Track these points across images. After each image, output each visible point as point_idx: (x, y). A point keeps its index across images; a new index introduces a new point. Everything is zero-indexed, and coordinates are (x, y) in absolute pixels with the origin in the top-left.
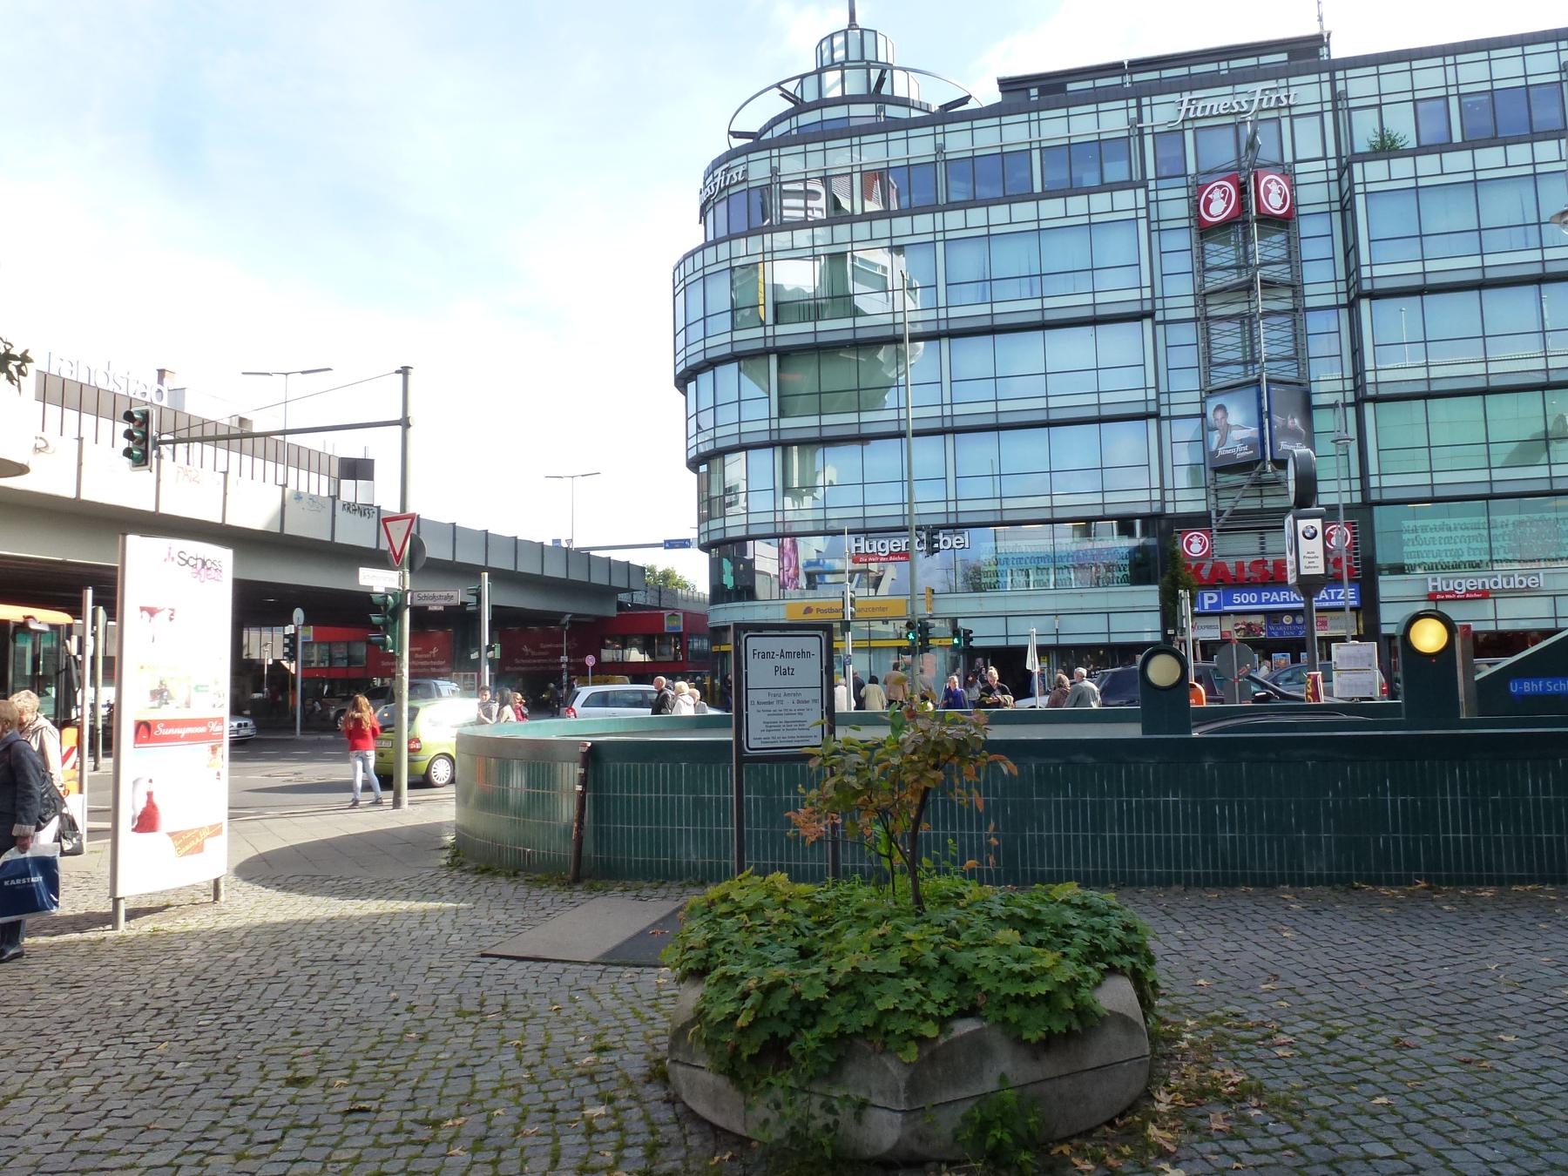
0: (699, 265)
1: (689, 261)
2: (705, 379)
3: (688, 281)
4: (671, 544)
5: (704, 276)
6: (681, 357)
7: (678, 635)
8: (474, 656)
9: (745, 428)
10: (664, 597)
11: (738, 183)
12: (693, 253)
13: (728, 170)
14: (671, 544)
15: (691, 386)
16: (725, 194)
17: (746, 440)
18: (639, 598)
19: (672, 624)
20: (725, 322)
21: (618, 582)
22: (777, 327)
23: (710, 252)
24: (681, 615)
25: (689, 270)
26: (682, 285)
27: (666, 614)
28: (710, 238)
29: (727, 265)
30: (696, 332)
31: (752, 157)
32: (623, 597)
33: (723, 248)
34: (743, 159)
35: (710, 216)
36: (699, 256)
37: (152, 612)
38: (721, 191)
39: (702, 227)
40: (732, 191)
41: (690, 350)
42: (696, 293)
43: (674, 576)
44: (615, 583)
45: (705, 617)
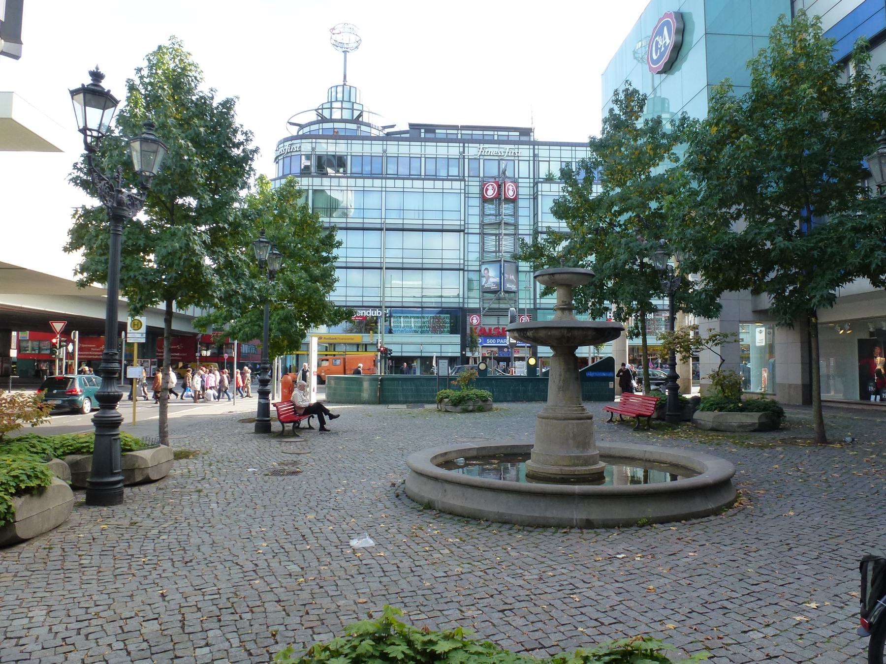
16: (290, 154)
31: (303, 141)
34: (299, 141)
35: (281, 162)
40: (293, 154)
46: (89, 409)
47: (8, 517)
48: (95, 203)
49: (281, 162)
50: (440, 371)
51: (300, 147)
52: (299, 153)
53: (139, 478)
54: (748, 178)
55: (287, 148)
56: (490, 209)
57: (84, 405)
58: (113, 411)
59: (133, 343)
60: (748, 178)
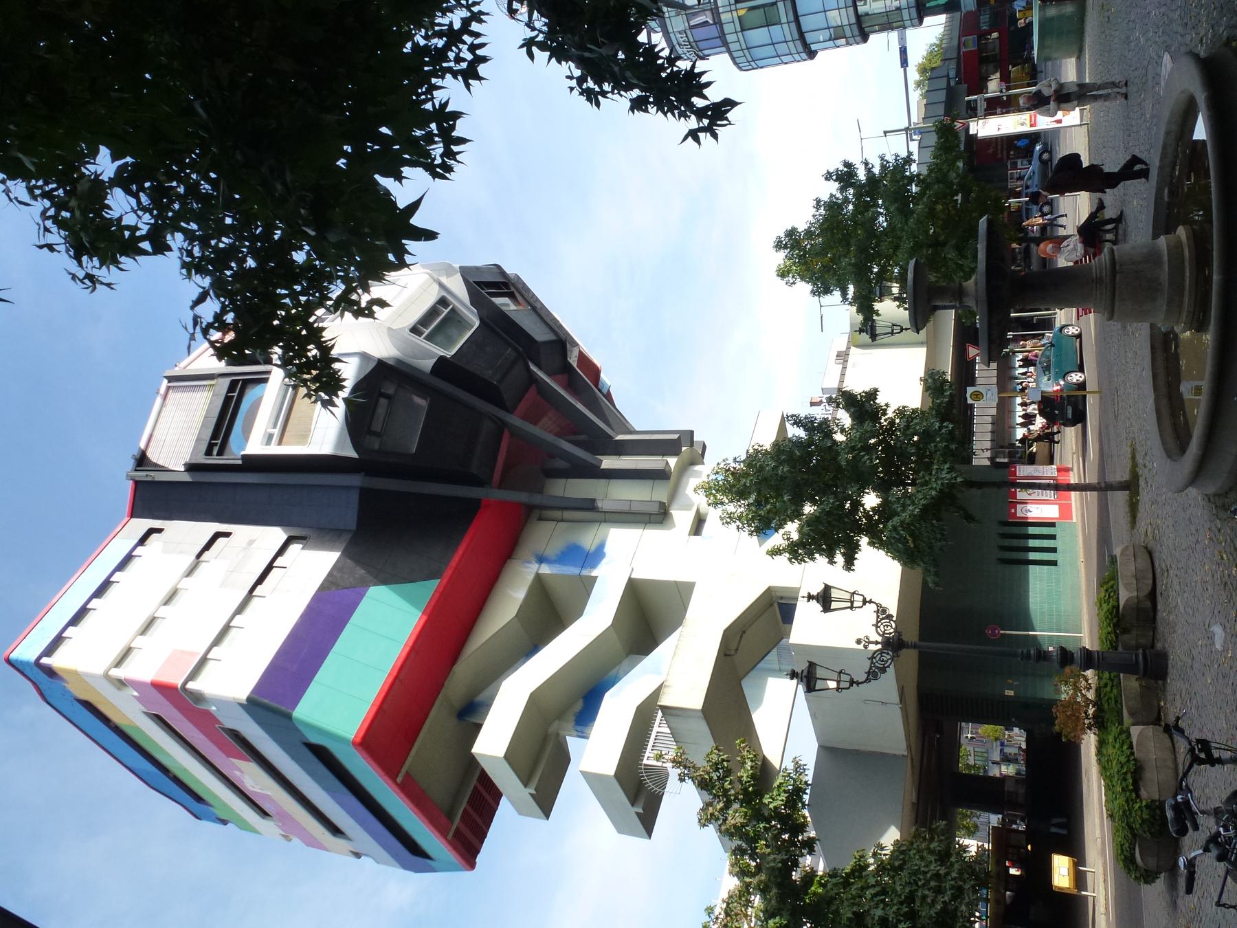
0: (741, 53)
1: (738, 60)
2: (809, 37)
3: (750, 59)
4: (904, 63)
5: (748, 49)
6: (797, 57)
7: (980, 38)
8: (1005, 98)
9: (789, 38)
10: (948, 56)
11: (687, 36)
12: (733, 59)
13: (680, 45)
14: (904, 63)
15: (813, 47)
16: (694, 44)
17: (796, 36)
18: (952, 74)
19: (971, 44)
20: (776, 29)
21: (943, 83)
22: (737, 5)
23: (733, 47)
24: (963, 39)
25: (744, 59)
26: (752, 63)
27: (963, 49)
28: (724, 49)
29: (740, 34)
30: (782, 48)
31: (670, 30)
32: (952, 83)
33: (730, 38)
34: (672, 36)
35: (706, 52)
36: (735, 54)
37: (999, 129)
38: (692, 47)
39: (711, 58)
40: (692, 40)
41: (794, 51)
42: (758, 53)
43: (923, 63)
44: (944, 85)
45: (969, 13)
46: (1080, 374)
47: (1153, 807)
48: (864, 541)
49: (706, 52)
50: (1037, 568)
51: (680, 33)
52: (688, 32)
53: (1148, 604)
54: (779, 495)
55: (685, 50)
56: (856, 604)
57: (1075, 381)
58: (1075, 655)
59: (999, 397)
60: (779, 495)
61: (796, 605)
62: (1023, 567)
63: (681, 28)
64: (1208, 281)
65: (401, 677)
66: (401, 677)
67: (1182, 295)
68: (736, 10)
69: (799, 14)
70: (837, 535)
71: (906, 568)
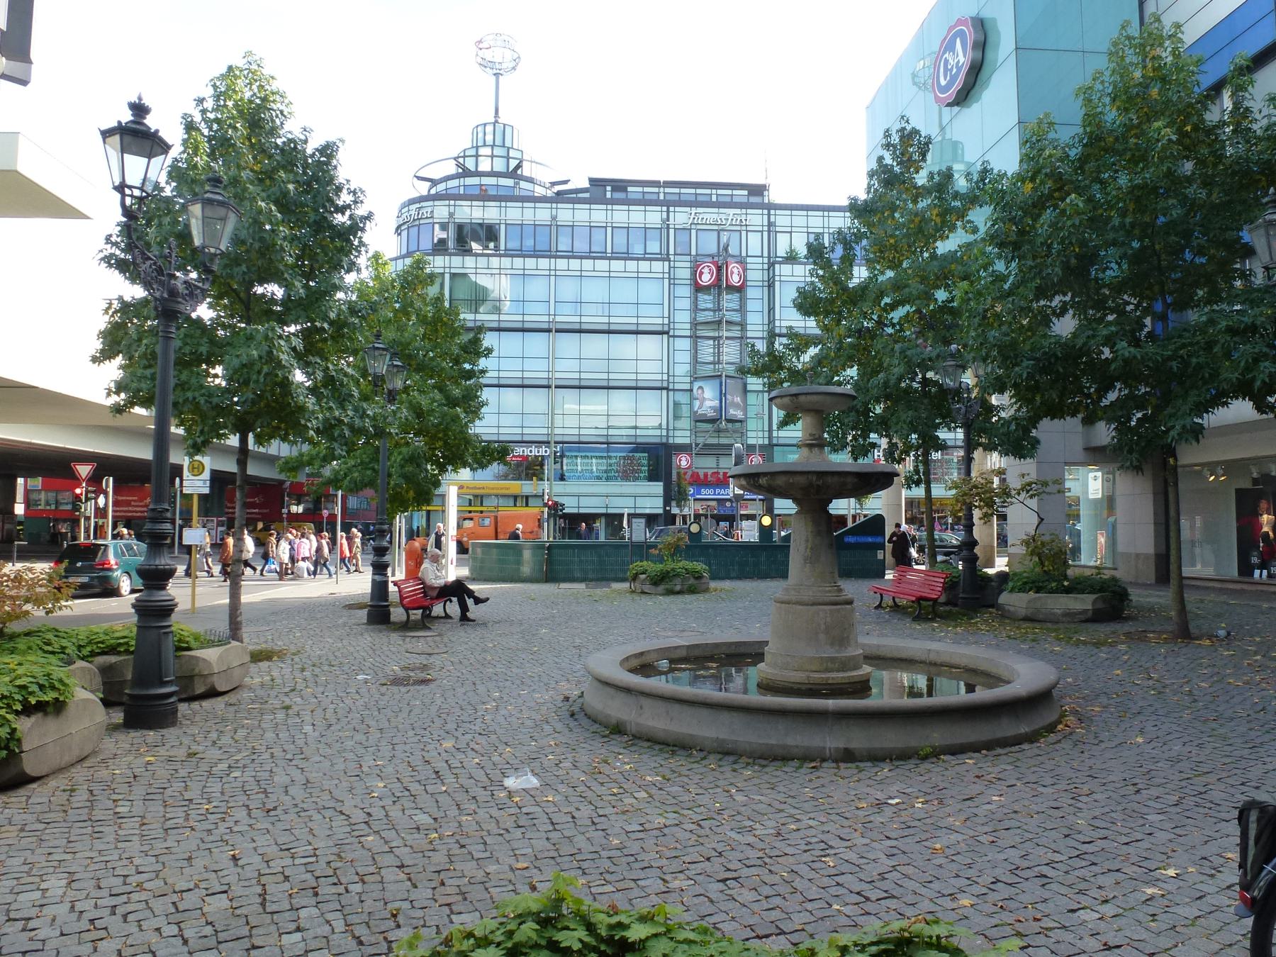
16: (417, 223)
31: (437, 203)
34: (430, 203)
35: (404, 234)
40: (422, 222)
46: (128, 589)
49: (404, 234)
51: (432, 212)
52: (430, 221)
55: (413, 213)
61: (458, 553)
62: (243, 609)
63: (436, 215)
64: (826, 696)
65: (829, 480)
66: (829, 480)
67: (838, 671)
68: (492, 156)
69: (489, 169)
70: (1147, 429)
71: (227, 608)
